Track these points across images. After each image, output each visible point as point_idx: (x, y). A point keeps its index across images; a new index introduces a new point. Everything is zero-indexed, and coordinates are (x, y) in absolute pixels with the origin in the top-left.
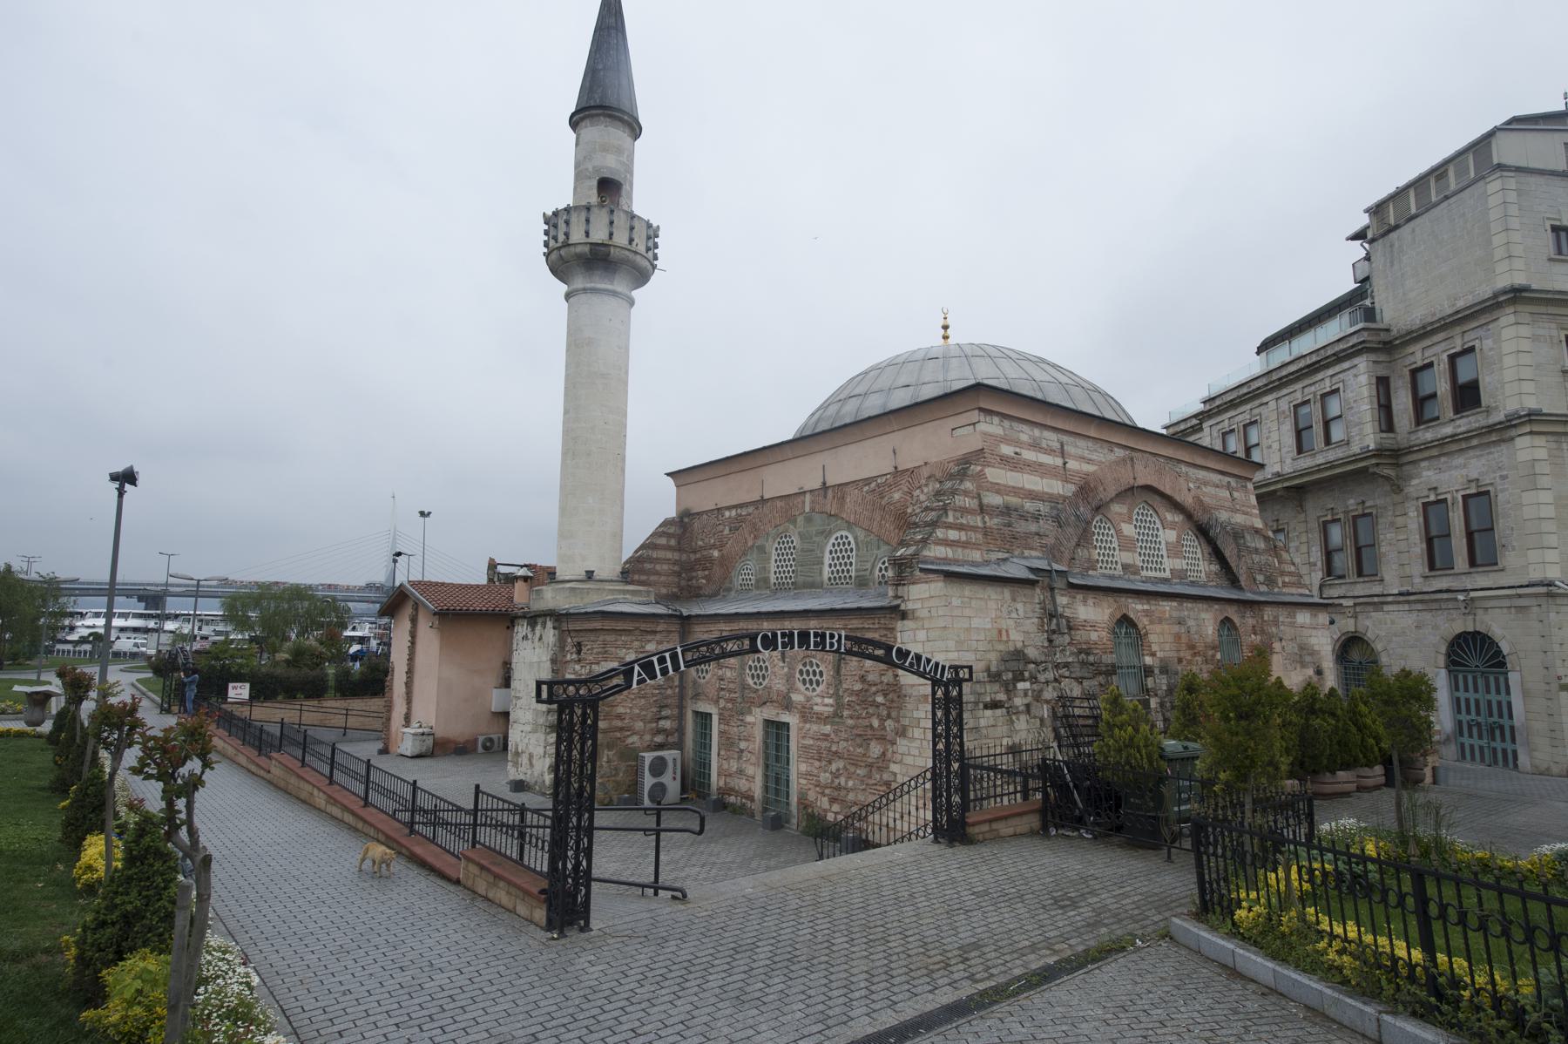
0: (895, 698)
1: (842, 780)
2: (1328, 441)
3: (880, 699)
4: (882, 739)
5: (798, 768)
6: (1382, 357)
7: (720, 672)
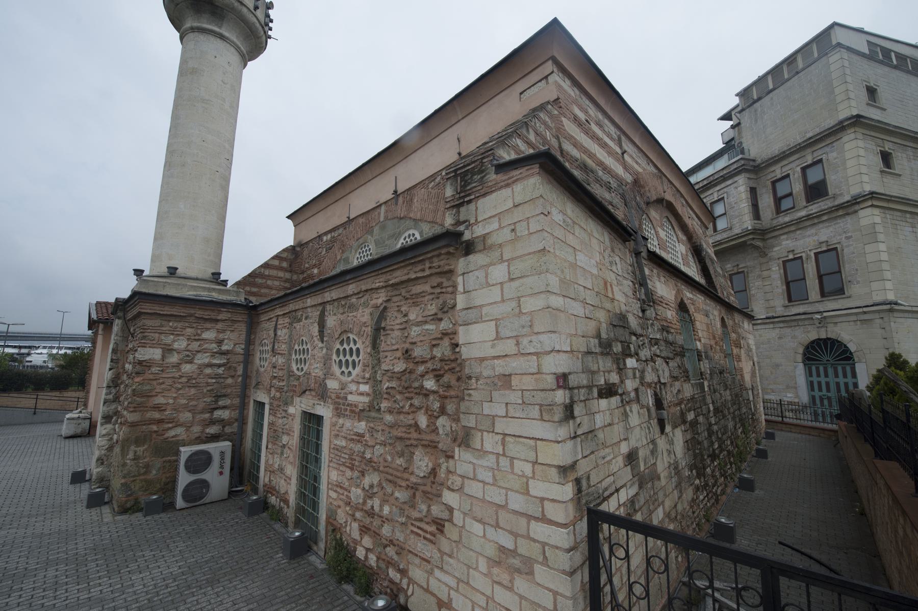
0: (454, 382)
1: (376, 502)
2: (715, 230)
3: (430, 384)
4: (432, 446)
5: (329, 474)
6: (752, 176)
7: (274, 359)
